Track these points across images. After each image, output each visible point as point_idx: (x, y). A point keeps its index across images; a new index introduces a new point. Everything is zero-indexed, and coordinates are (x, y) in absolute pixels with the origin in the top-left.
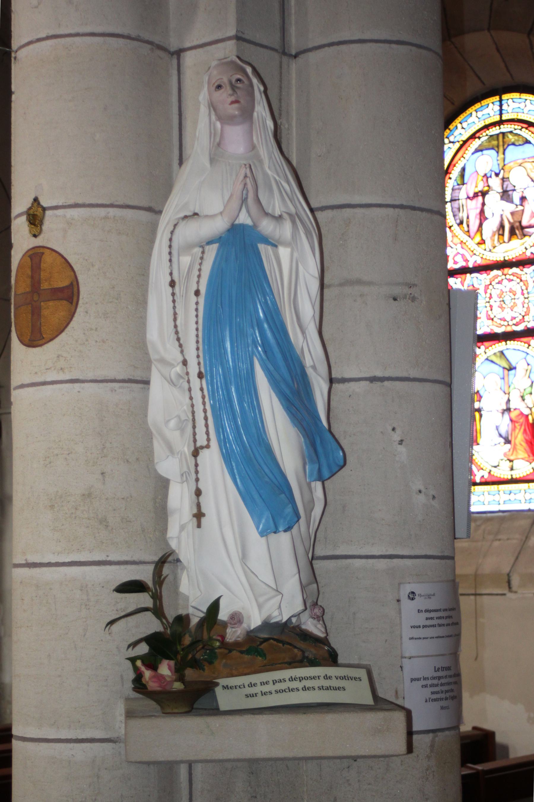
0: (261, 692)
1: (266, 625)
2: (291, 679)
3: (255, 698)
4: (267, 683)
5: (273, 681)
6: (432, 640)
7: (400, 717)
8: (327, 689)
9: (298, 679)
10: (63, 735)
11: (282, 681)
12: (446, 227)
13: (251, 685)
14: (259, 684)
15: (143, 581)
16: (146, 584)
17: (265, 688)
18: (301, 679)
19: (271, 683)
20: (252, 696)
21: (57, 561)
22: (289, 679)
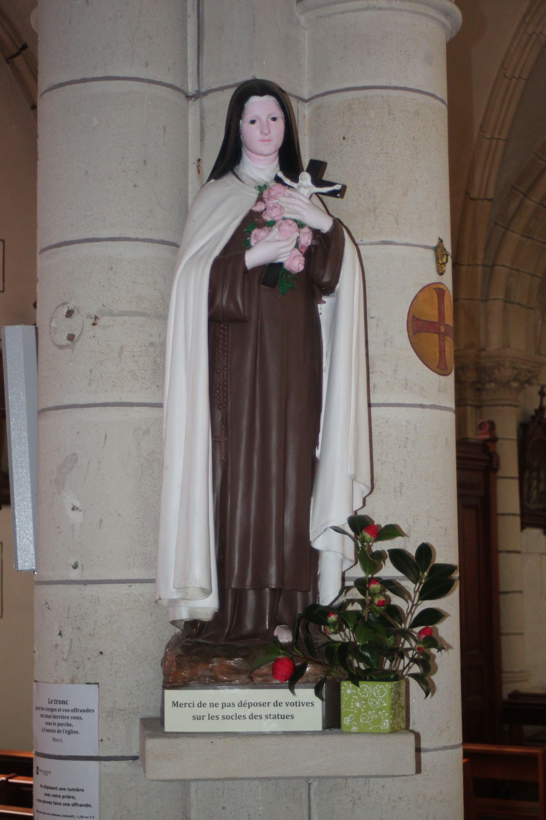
2: (241, 704)
3: (201, 721)
4: (216, 705)
5: (223, 704)
6: (44, 812)
8: (275, 717)
9: (247, 705)
11: (231, 705)
12: (426, 585)
13: (201, 705)
14: (208, 705)
15: (399, 607)
16: (402, 610)
18: (250, 705)
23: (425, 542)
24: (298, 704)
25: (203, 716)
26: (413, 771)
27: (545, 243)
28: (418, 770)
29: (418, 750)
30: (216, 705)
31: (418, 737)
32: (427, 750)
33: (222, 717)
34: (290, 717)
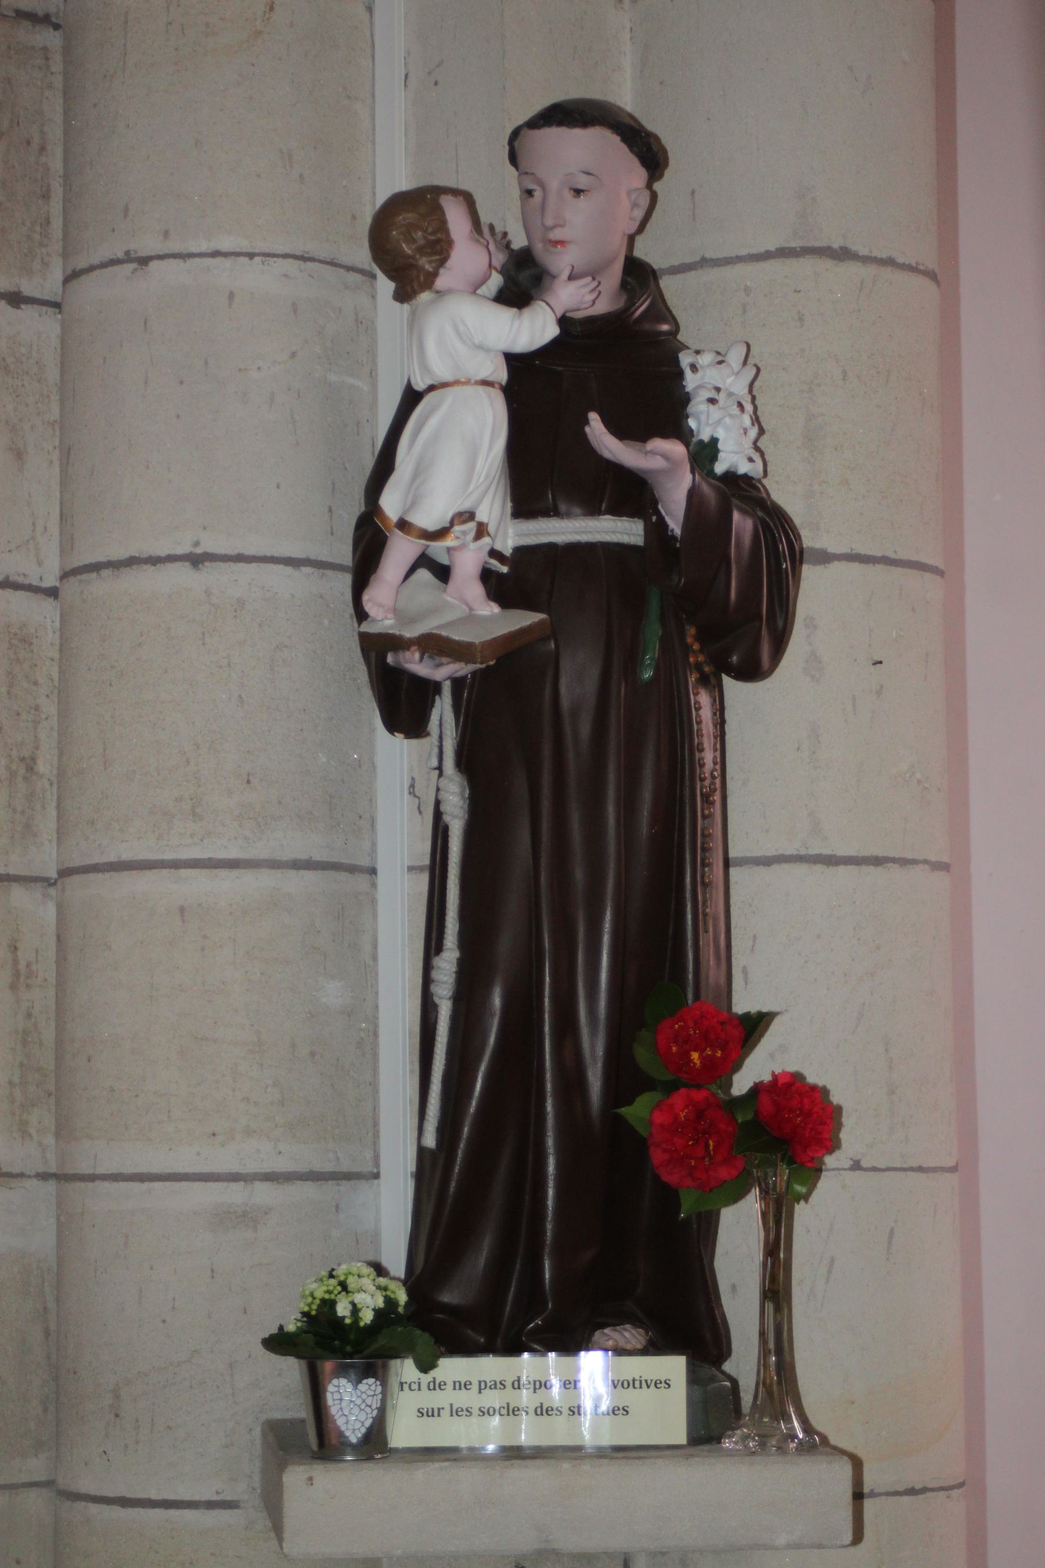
0: (451, 1405)
1: (544, 1354)
3: (436, 1418)
4: (466, 1386)
5: (480, 1382)
7: (844, 1471)
10: (188, 1514)
11: (499, 1385)
17: (462, 1399)
19: (475, 1387)
20: (432, 1413)
21: (669, 148)
22: (513, 1384)
23: (828, 1087)
24: (637, 1384)
25: (439, 1409)
26: (848, 1537)
27: (7, 584)
28: (858, 1537)
29: (858, 1496)
30: (466, 1386)
31: (857, 1464)
32: (873, 1494)
33: (480, 1410)
34: (664, 1385)
